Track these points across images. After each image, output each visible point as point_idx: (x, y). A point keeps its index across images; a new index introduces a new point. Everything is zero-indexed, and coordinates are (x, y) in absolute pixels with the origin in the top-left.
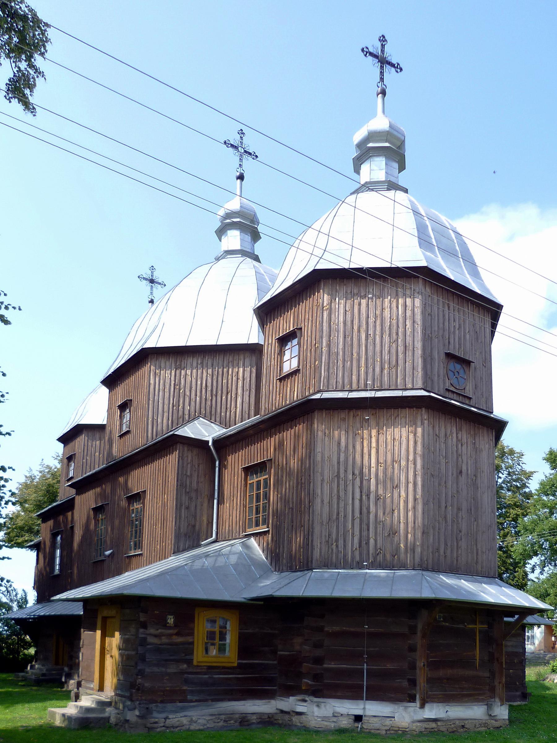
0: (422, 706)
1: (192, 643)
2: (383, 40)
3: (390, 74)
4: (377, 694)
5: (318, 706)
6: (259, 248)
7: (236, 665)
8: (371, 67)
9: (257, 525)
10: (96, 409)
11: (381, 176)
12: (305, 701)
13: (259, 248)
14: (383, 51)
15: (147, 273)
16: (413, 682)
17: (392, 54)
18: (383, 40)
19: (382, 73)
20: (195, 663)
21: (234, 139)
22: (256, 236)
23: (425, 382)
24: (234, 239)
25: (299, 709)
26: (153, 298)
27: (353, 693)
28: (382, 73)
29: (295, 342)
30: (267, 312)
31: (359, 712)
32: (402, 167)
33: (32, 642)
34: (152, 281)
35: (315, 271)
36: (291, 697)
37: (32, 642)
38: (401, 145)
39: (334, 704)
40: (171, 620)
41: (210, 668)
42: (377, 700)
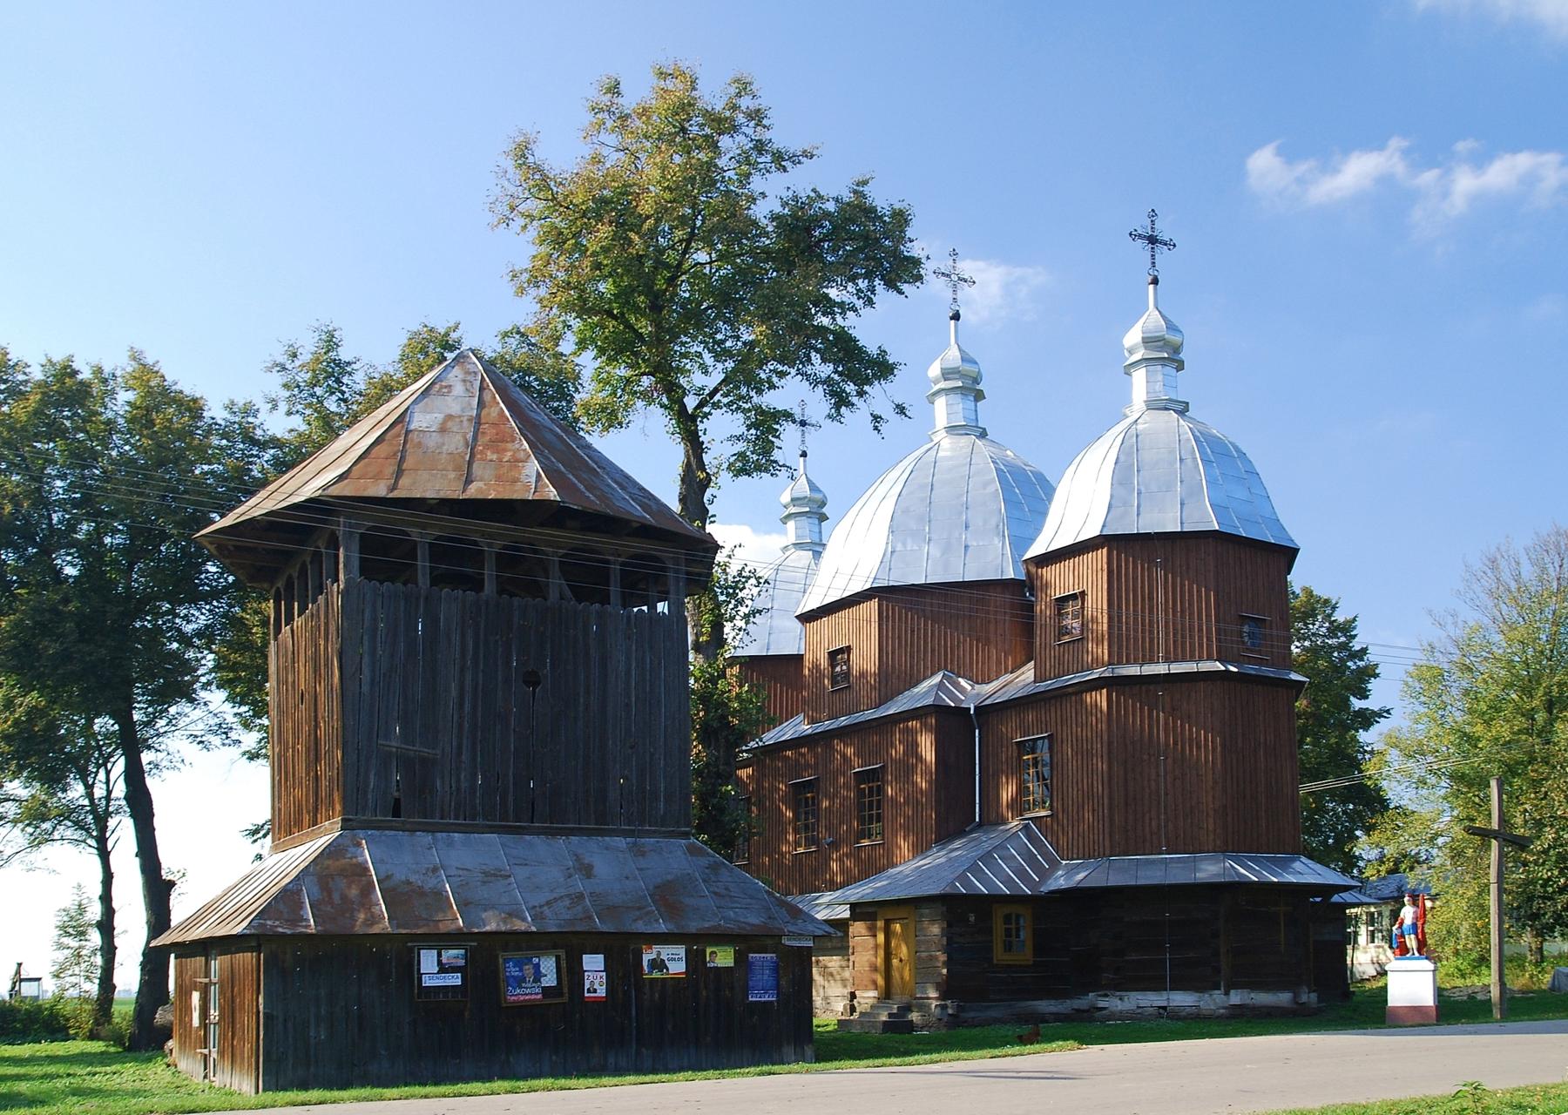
0: (1227, 993)
3: (1162, 253)
4: (1177, 986)
17: (1164, 231)
25: (1101, 1004)
27: (1157, 985)
34: (1153, 240)
38: (1177, 349)
40: (972, 919)
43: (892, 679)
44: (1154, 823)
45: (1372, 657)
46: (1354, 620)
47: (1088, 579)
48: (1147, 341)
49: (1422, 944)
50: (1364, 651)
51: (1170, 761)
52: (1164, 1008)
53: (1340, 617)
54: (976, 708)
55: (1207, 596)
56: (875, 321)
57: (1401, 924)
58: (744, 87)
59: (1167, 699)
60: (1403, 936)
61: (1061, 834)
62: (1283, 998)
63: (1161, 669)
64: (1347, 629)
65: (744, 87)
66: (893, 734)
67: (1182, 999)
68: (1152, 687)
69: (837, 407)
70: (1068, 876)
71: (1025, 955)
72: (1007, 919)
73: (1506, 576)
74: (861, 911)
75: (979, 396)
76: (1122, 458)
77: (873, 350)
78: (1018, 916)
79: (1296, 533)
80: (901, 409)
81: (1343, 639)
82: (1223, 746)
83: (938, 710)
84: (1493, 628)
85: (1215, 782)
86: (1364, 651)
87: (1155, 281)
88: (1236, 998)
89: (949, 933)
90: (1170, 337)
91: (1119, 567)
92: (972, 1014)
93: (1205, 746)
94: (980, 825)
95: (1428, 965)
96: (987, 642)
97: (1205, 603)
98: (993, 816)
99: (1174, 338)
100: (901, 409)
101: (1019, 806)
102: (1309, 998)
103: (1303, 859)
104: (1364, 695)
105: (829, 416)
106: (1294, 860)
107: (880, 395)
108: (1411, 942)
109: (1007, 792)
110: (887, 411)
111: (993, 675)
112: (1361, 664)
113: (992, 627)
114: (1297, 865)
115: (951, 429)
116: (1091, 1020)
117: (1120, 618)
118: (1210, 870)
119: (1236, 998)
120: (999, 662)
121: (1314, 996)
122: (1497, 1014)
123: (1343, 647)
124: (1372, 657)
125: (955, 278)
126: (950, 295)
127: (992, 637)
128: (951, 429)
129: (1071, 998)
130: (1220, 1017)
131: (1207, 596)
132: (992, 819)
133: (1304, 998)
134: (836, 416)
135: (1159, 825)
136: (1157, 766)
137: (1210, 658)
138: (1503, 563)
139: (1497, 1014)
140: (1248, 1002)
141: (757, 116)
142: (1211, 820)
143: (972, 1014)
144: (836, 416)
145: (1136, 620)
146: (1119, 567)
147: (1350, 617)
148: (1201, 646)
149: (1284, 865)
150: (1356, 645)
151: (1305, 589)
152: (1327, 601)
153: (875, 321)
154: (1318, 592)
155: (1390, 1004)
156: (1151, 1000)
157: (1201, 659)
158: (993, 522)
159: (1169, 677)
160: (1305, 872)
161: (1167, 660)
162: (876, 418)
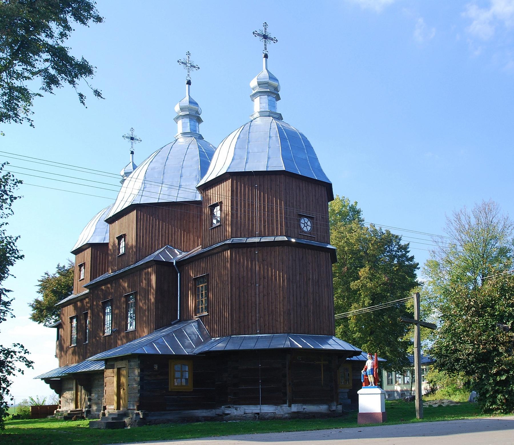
0: (290, 406)
1: (168, 379)
3: (270, 45)
4: (266, 402)
5: (236, 409)
7: (192, 390)
8: (260, 42)
10: (102, 235)
12: (230, 407)
15: (260, 29)
16: (285, 394)
20: (170, 390)
23: (286, 232)
25: (227, 412)
26: (267, 53)
27: (255, 402)
29: (219, 207)
33: (330, 406)
34: (265, 37)
37: (330, 406)
38: (276, 89)
39: (246, 408)
40: (156, 367)
41: (178, 392)
43: (141, 249)
45: (416, 261)
46: (408, 244)
47: (222, 193)
48: (260, 84)
50: (412, 258)
51: (261, 287)
52: (258, 414)
53: (402, 243)
54: (176, 262)
55: (281, 204)
57: (366, 369)
59: (260, 255)
60: (367, 376)
61: (211, 325)
62: (323, 408)
63: (256, 240)
64: (405, 248)
66: (141, 275)
67: (267, 409)
68: (253, 249)
69: (49, 85)
70: (219, 345)
73: (464, 222)
74: (109, 363)
75: (199, 120)
76: (241, 136)
77: (78, 59)
80: (97, 93)
81: (404, 253)
82: (288, 279)
83: (157, 263)
84: (458, 244)
85: (284, 298)
86: (412, 258)
87: (266, 56)
88: (295, 408)
89: (141, 375)
90: (271, 82)
91: (237, 188)
92: (155, 418)
93: (280, 278)
94: (180, 321)
95: (378, 391)
96: (189, 232)
97: (279, 207)
98: (185, 317)
99: (274, 83)
100: (97, 93)
101: (197, 310)
107: (83, 83)
109: (191, 303)
111: (191, 248)
112: (411, 263)
113: (191, 224)
114: (331, 341)
115: (184, 134)
116: (223, 420)
117: (237, 214)
119: (295, 408)
120: (194, 241)
121: (340, 407)
122: (418, 416)
123: (404, 256)
124: (416, 261)
125: (189, 65)
127: (191, 229)
128: (184, 134)
130: (286, 418)
131: (281, 204)
132: (186, 318)
133: (334, 408)
135: (256, 319)
136: (255, 289)
137: (281, 235)
138: (463, 218)
139: (418, 416)
140: (302, 410)
142: (282, 317)
143: (155, 418)
145: (245, 216)
146: (237, 188)
147: (406, 243)
148: (277, 229)
150: (409, 255)
151: (386, 231)
152: (397, 237)
154: (393, 232)
155: (361, 411)
156: (252, 409)
157: (277, 236)
158: (194, 174)
159: (259, 243)
161: (260, 236)
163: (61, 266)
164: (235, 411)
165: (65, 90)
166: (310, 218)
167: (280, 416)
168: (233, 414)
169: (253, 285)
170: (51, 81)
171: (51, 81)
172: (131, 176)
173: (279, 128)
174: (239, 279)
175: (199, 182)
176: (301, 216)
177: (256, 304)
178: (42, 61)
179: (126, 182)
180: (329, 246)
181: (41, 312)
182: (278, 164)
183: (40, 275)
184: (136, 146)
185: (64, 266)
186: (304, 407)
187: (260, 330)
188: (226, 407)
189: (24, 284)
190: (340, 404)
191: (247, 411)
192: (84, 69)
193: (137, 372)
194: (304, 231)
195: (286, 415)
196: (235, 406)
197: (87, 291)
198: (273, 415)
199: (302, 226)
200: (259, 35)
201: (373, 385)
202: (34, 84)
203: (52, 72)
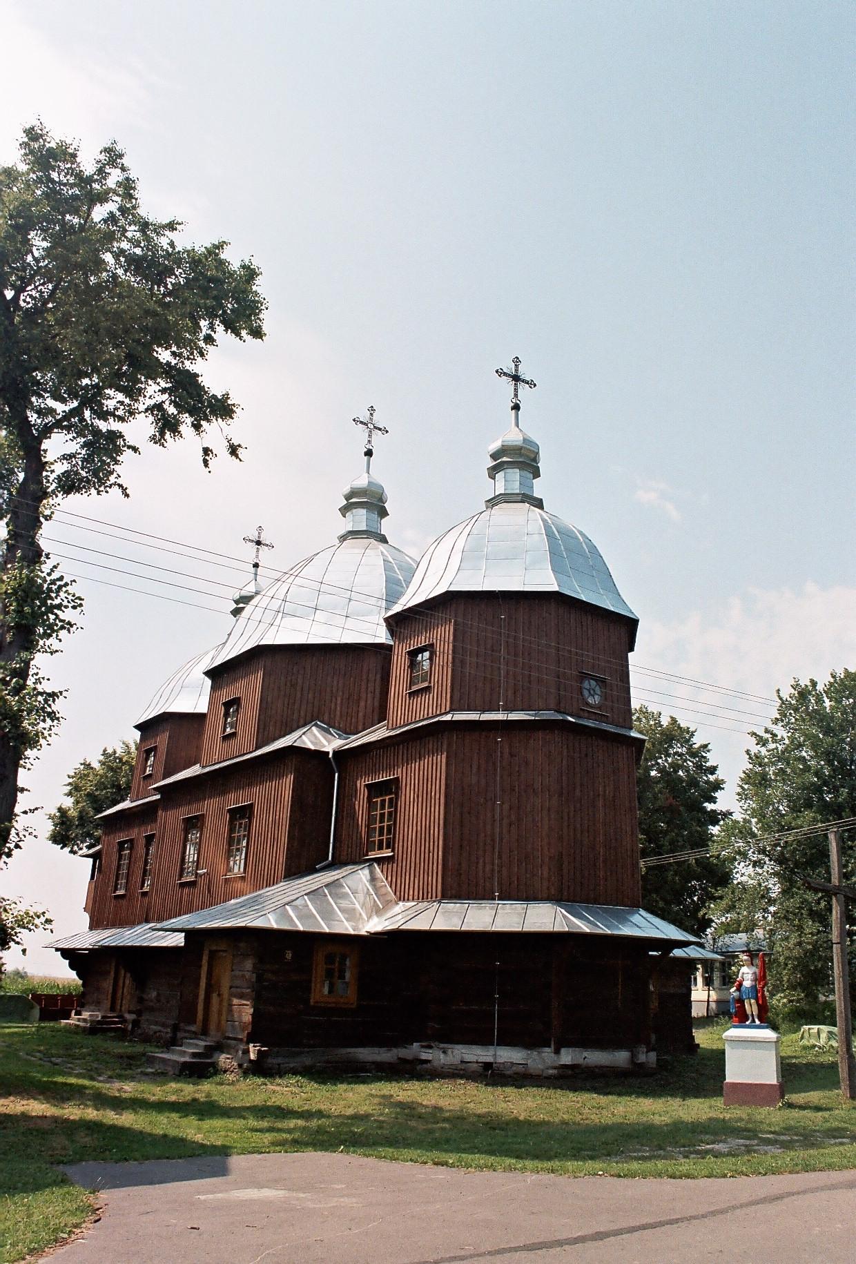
0: (557, 1052)
1: (310, 981)
2: (517, 361)
3: (523, 389)
4: (505, 1041)
5: (444, 1052)
6: (386, 526)
8: (507, 385)
9: (380, 848)
10: (194, 698)
11: (516, 488)
12: (430, 1047)
13: (386, 526)
14: (516, 370)
17: (524, 372)
18: (517, 361)
19: (516, 390)
21: (365, 416)
22: (383, 513)
24: (360, 518)
25: (424, 1056)
27: (482, 1038)
28: (516, 390)
29: (427, 654)
30: (397, 623)
31: (490, 1059)
32: (536, 474)
35: (447, 592)
36: (697, 1041)
40: (289, 955)
42: (515, 1046)
44: (488, 868)
49: (763, 1010)
51: (506, 807)
53: (698, 741)
54: (335, 753)
56: (221, 364)
57: (741, 984)
58: (113, 156)
62: (621, 1057)
65: (113, 156)
67: (508, 1056)
71: (348, 993)
72: (330, 959)
78: (344, 957)
79: (633, 602)
102: (648, 1058)
103: (642, 912)
104: (713, 800)
105: (153, 438)
106: (633, 913)
107: (215, 431)
108: (751, 1007)
110: (221, 449)
114: (636, 918)
118: (544, 917)
121: (653, 1056)
124: (720, 775)
126: (367, 439)
129: (396, 1046)
133: (642, 1058)
134: (158, 439)
135: (493, 870)
136: (493, 810)
140: (581, 1061)
141: (128, 187)
144: (158, 439)
149: (623, 920)
153: (221, 364)
156: (477, 1054)
160: (645, 925)
161: (508, 709)
162: (206, 451)
163: (110, 751)
164: (442, 1056)
165: (188, 442)
166: (602, 682)
167: (538, 1072)
168: (435, 1063)
169: (489, 803)
170: (167, 426)
171: (167, 426)
172: (254, 602)
173: (544, 520)
174: (463, 789)
175: (387, 609)
176: (583, 676)
177: (493, 840)
178: (154, 391)
179: (245, 614)
180: (634, 734)
181: (65, 832)
182: (544, 580)
183: (73, 765)
184: (265, 555)
185: (115, 752)
186: (585, 1054)
187: (501, 893)
188: (422, 1047)
189: (44, 783)
190: (653, 1050)
191: (468, 1058)
192: (223, 409)
193: (249, 964)
194: (588, 704)
195: (551, 1071)
196: (442, 1045)
197: (158, 797)
198: (521, 1069)
199: (586, 693)
200: (505, 374)
201: (758, 1022)
202: (139, 429)
203: (172, 410)
